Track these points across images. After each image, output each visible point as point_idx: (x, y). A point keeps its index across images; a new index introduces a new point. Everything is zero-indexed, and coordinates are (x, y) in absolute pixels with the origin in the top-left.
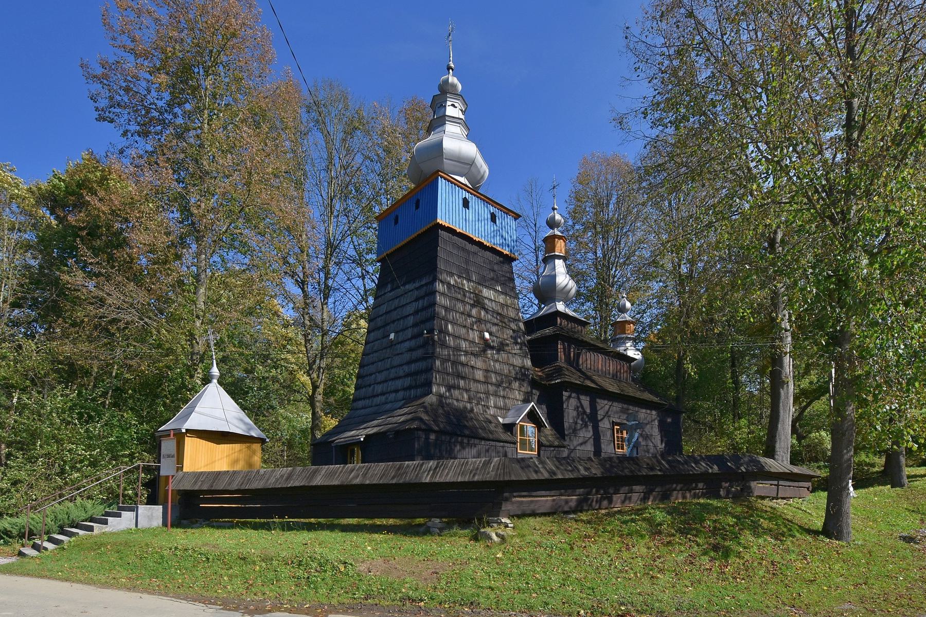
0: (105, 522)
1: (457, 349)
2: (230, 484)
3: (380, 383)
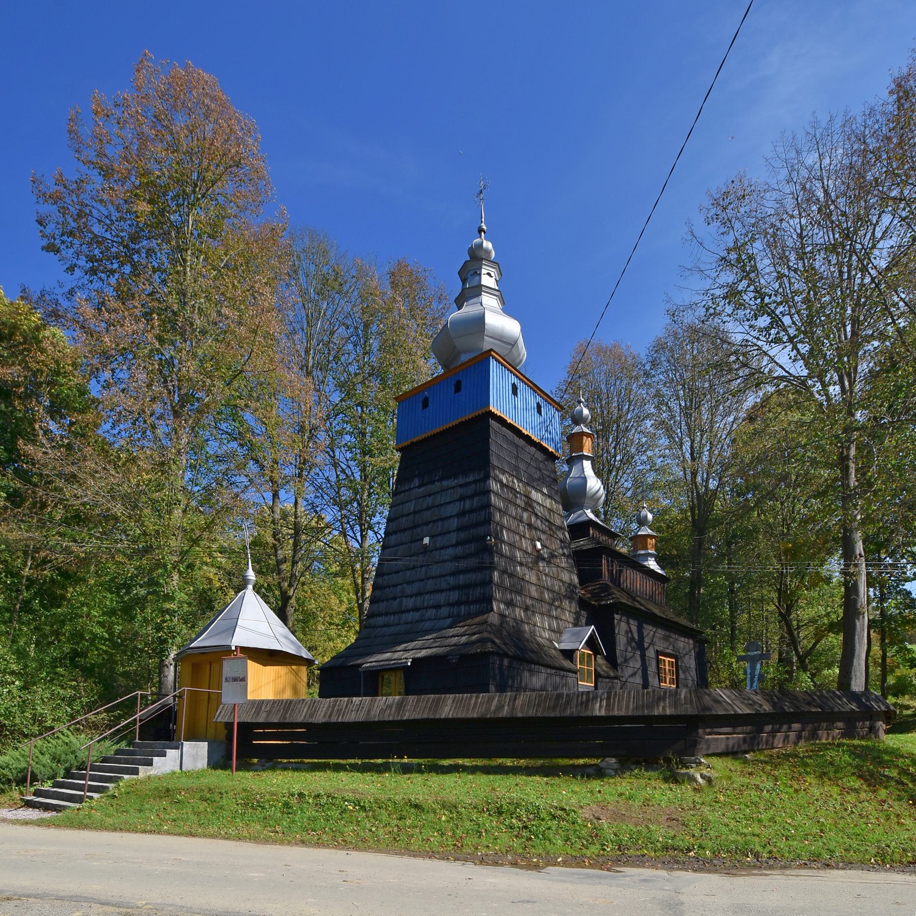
0: (150, 763)
1: (512, 559)
2: (311, 715)
3: (411, 596)
